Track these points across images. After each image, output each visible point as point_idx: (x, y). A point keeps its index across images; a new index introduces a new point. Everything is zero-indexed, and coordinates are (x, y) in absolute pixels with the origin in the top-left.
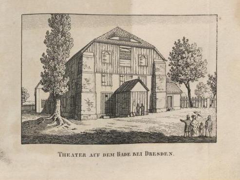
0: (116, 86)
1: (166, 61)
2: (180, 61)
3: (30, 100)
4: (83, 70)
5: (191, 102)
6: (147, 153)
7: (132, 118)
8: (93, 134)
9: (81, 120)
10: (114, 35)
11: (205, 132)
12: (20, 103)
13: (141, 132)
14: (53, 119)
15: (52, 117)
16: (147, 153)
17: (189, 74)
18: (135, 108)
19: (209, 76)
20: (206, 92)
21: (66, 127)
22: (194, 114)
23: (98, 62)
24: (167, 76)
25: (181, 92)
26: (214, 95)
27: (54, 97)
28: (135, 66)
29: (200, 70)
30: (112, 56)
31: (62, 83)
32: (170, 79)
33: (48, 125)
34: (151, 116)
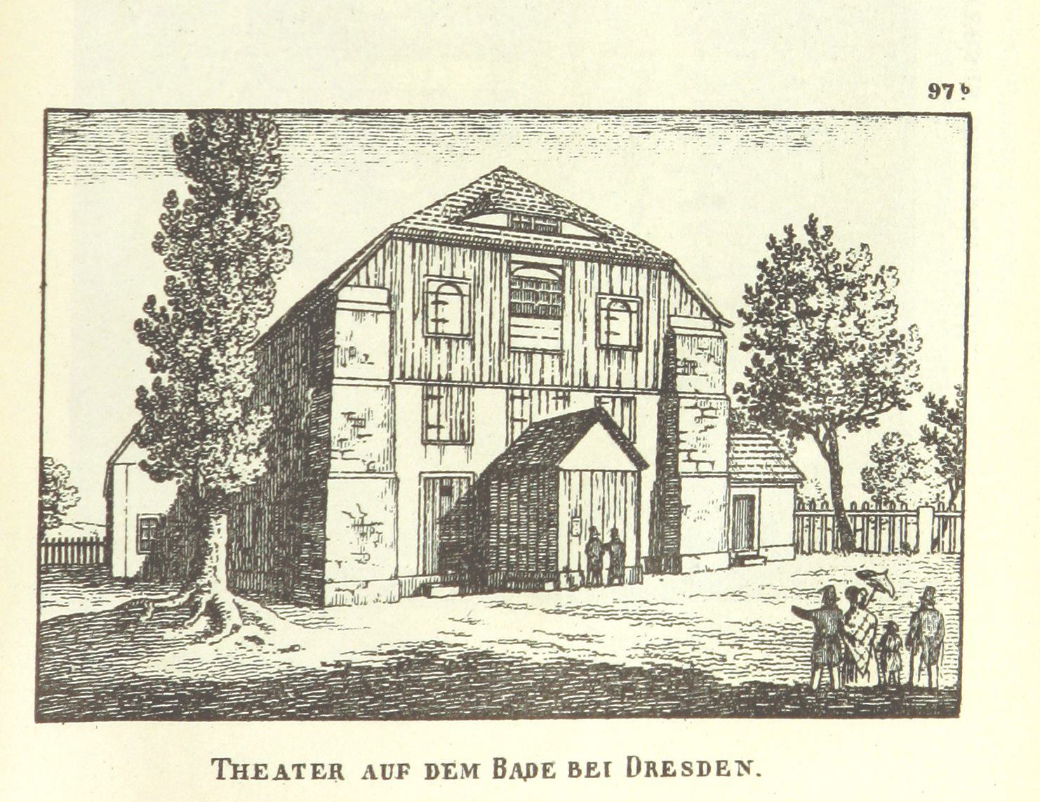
0: (490, 444)
1: (730, 325)
2: (793, 328)
3: (82, 517)
4: (338, 371)
5: (843, 526)
6: (634, 766)
7: (565, 598)
8: (378, 671)
9: (321, 603)
10: (484, 204)
11: (907, 668)
12: (35, 532)
13: (606, 666)
14: (192, 607)
15: (186, 596)
16: (634, 766)
17: (835, 391)
18: (578, 547)
19: (929, 401)
20: (916, 477)
21: (254, 639)
22: (860, 584)
23: (407, 334)
24: (734, 398)
25: (797, 481)
26: (954, 496)
27: (196, 507)
28: (583, 348)
29: (885, 374)
30: (472, 304)
31: (237, 439)
32: (747, 415)
33: (169, 634)
34: (656, 587)
